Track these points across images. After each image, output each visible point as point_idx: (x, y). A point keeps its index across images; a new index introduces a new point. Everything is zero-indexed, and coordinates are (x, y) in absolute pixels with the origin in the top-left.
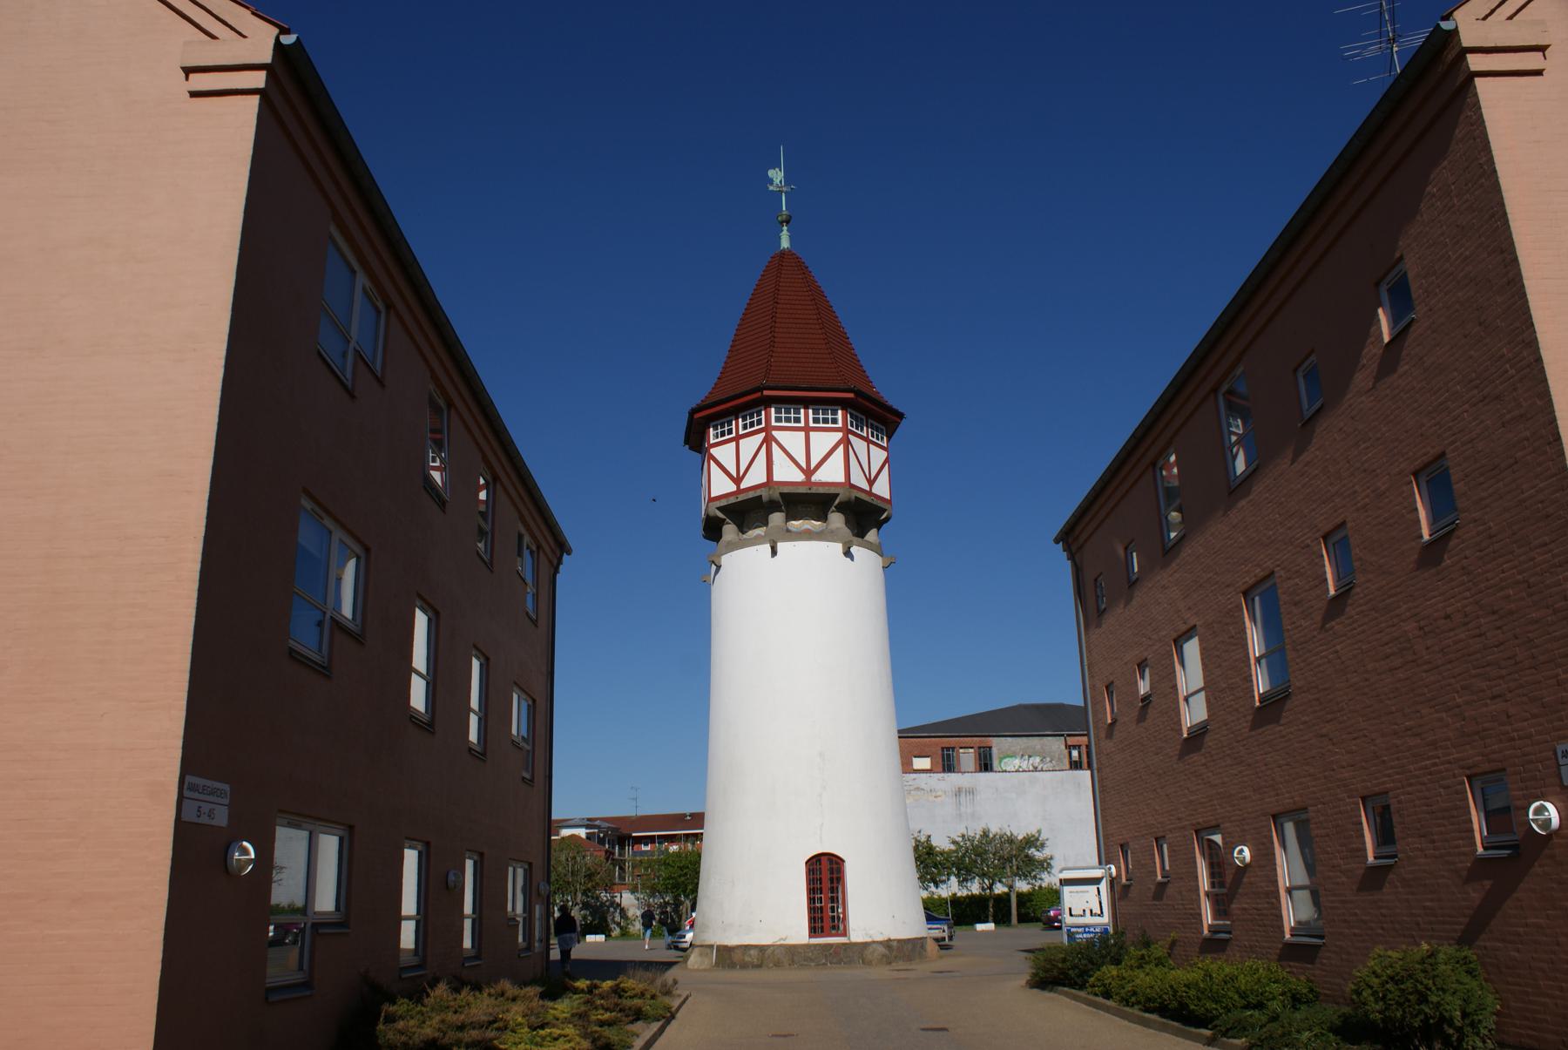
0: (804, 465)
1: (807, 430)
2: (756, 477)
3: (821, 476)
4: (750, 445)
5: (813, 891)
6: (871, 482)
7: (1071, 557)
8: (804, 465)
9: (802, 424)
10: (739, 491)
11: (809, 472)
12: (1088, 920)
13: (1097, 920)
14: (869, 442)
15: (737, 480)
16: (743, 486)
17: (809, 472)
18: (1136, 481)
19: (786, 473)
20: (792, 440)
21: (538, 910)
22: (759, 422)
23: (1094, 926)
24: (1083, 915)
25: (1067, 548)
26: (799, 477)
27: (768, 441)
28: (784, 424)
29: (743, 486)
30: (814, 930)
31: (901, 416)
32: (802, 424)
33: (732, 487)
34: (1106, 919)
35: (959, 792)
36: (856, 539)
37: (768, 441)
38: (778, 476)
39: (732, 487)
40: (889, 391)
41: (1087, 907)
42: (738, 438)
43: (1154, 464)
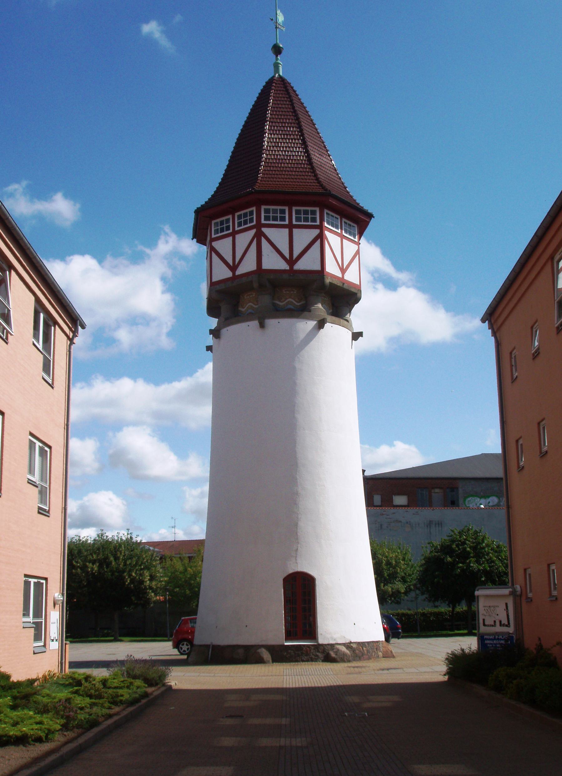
0: (287, 256)
1: (291, 227)
2: (248, 265)
3: (300, 265)
4: (243, 239)
5: (289, 601)
6: (343, 270)
7: (494, 334)
8: (287, 256)
9: (287, 222)
10: (234, 277)
11: (291, 261)
12: (498, 629)
13: (505, 629)
14: (342, 237)
15: (233, 268)
16: (239, 272)
17: (291, 261)
18: (539, 273)
19: (273, 262)
20: (279, 236)
21: (491, 637)
22: (251, 220)
23: (502, 633)
24: (494, 625)
25: (491, 327)
26: (283, 265)
27: (259, 235)
28: (271, 222)
29: (239, 272)
30: (289, 637)
31: (370, 216)
32: (287, 222)
33: (229, 274)
34: (511, 630)
35: (430, 524)
36: (329, 318)
37: (259, 235)
38: (267, 265)
39: (229, 274)
40: (363, 198)
41: (497, 619)
42: (234, 234)
43: (552, 258)
